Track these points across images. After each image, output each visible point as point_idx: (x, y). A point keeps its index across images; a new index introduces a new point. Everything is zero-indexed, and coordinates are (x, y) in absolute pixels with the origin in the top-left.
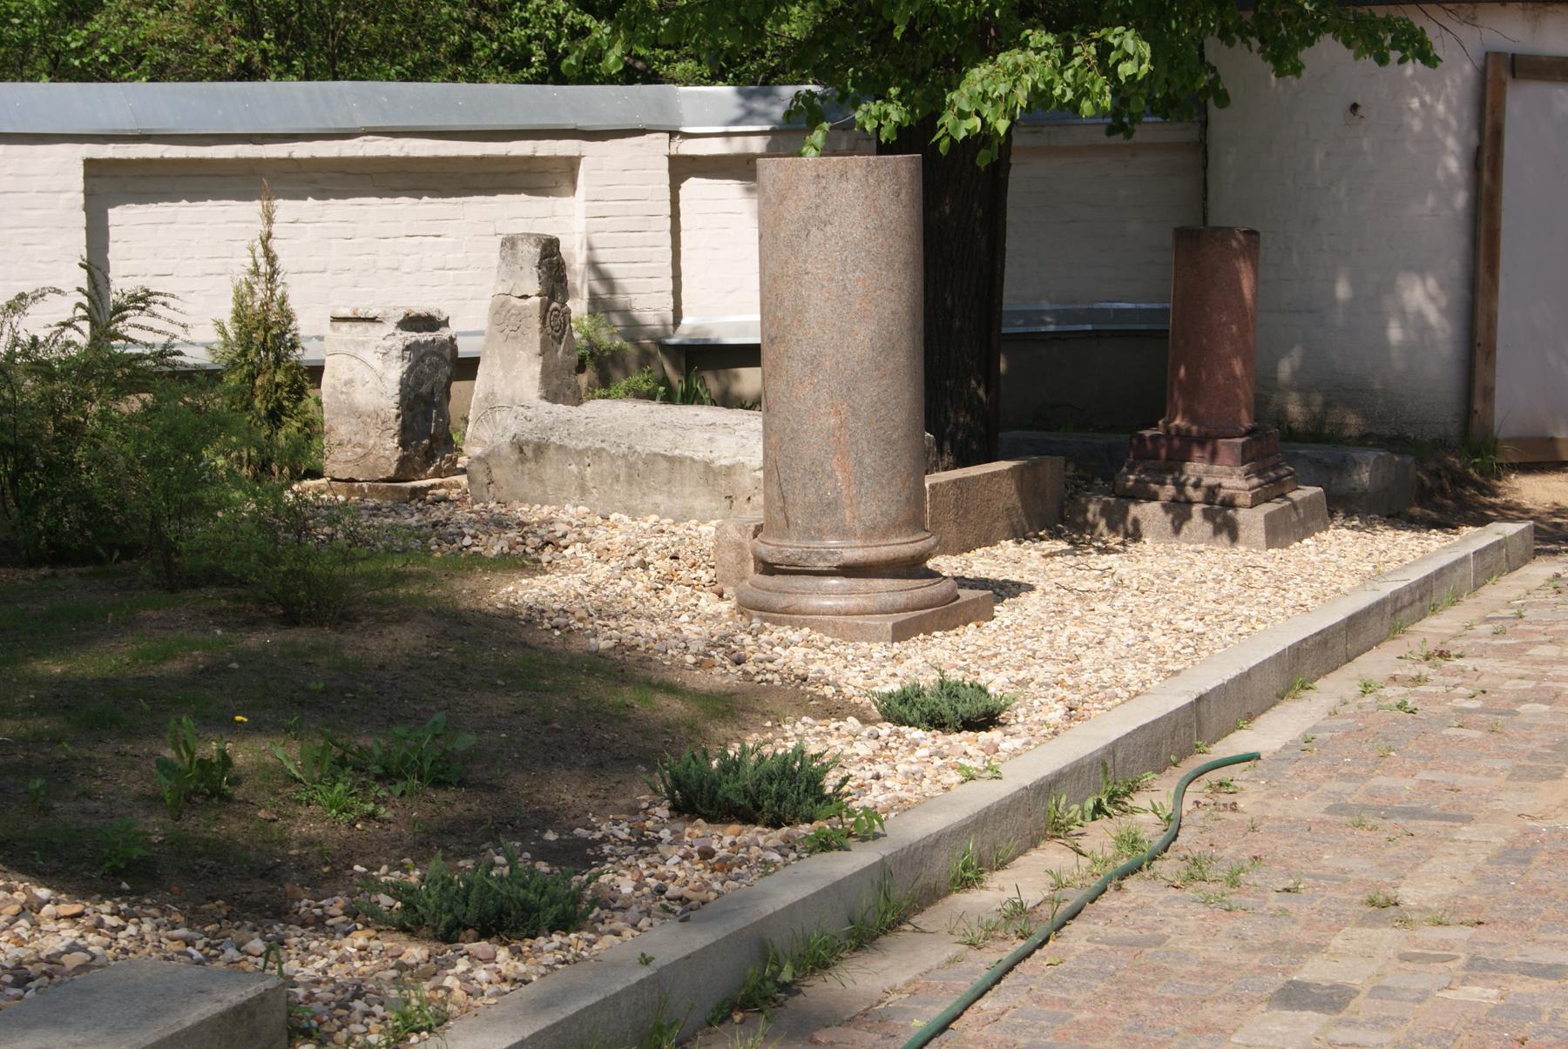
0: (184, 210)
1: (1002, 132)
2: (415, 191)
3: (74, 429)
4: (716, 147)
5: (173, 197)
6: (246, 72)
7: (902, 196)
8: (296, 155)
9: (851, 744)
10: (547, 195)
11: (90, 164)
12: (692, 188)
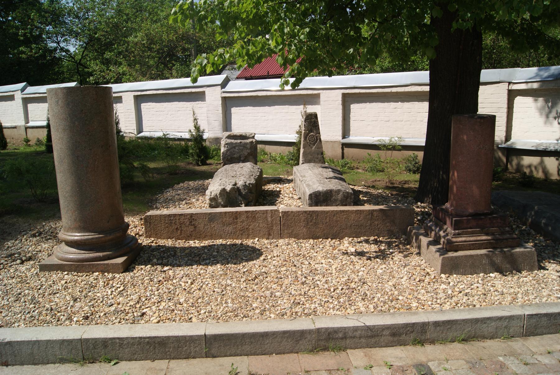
0: (368, 105)
1: (294, 79)
4: (523, 87)
7: (60, 103)
11: (134, 96)
12: (145, 106)
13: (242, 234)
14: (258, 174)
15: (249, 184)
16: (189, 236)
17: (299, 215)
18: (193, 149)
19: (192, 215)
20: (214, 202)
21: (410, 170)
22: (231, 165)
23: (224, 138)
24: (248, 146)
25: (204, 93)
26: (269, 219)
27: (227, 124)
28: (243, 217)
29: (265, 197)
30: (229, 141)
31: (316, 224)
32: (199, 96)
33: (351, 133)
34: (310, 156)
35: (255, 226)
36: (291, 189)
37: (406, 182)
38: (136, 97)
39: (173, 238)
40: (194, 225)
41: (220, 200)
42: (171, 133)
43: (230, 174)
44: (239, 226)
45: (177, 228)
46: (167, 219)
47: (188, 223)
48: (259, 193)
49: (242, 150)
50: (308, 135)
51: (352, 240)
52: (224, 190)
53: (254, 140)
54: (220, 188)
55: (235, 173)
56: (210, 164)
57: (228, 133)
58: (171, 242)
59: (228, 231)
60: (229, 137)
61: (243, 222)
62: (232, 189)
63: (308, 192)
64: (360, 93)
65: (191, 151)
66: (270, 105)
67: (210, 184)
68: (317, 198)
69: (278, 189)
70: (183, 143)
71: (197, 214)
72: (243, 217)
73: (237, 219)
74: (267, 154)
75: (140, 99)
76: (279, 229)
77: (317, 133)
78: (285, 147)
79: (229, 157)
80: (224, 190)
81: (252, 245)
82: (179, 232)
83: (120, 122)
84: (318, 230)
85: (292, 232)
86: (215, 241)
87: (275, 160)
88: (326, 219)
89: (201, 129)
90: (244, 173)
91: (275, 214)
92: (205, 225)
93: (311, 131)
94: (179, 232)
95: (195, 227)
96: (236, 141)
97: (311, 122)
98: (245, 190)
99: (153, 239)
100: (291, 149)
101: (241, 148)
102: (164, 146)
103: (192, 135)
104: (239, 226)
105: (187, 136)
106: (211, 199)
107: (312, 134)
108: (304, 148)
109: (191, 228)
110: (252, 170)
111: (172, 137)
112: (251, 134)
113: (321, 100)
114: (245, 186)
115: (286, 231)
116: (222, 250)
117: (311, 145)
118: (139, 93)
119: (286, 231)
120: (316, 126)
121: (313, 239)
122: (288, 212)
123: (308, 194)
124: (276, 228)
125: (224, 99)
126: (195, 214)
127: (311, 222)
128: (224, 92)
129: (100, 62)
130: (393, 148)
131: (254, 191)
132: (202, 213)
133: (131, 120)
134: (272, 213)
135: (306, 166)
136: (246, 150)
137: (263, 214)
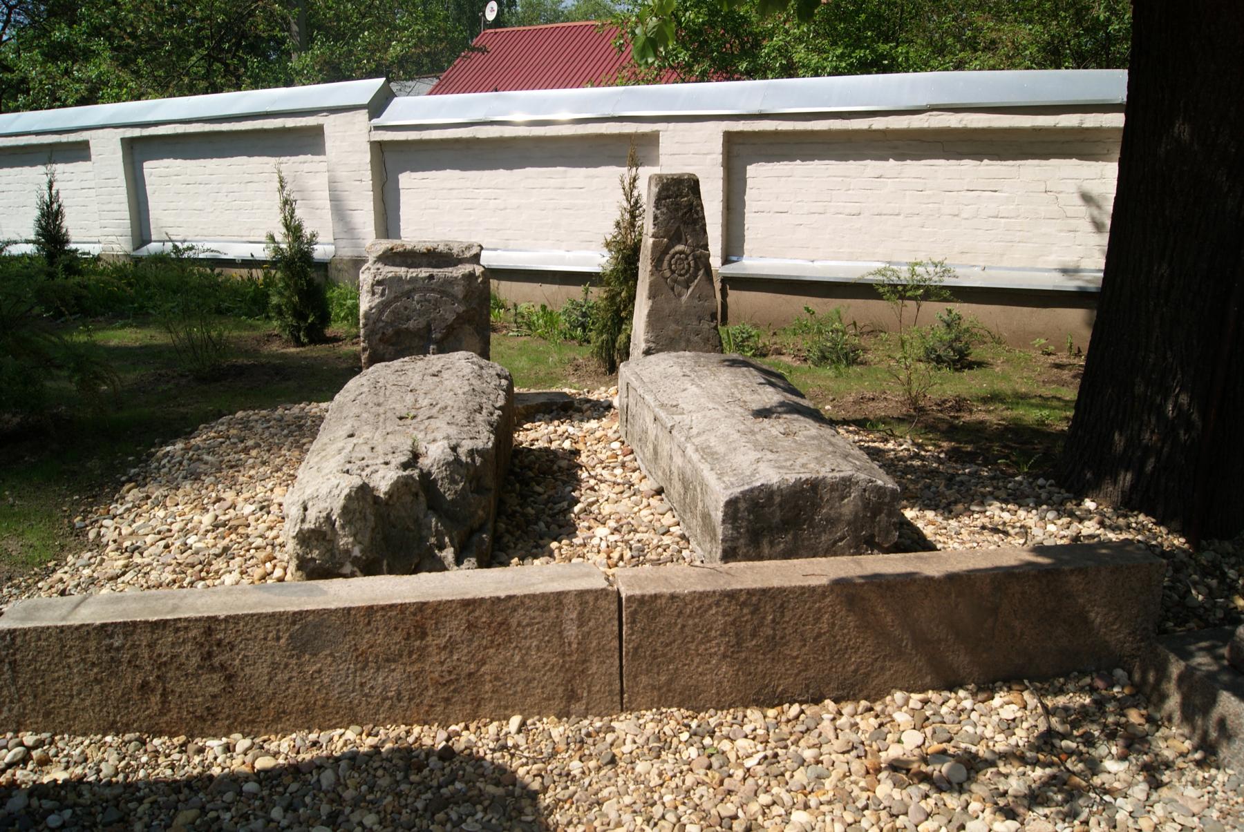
2: (978, 155)
3: (269, 451)
5: (791, 158)
6: (993, 68)
8: (875, 127)
9: (112, 658)
10: (1097, 160)
12: (154, 170)
13: (447, 700)
14: (501, 402)
15: (471, 453)
16: (202, 719)
17: (702, 612)
18: (281, 294)
19: (210, 625)
20: (320, 556)
21: (939, 360)
22: (397, 363)
23: (371, 259)
24: (459, 290)
25: (318, 131)
26: (572, 631)
27: (387, 220)
28: (454, 628)
29: (525, 483)
30: (389, 271)
31: (774, 644)
32: (304, 140)
33: (746, 246)
34: (673, 326)
35: (507, 661)
36: (616, 445)
37: (960, 404)
38: (130, 145)
39: (127, 728)
40: (223, 667)
41: (345, 541)
42: (199, 246)
43: (390, 404)
44: (434, 665)
45: (144, 686)
46: (92, 644)
47: (195, 660)
48: (514, 498)
49: (437, 304)
50: (665, 251)
51: (925, 702)
52: (364, 492)
53: (479, 270)
54: (349, 483)
55: (409, 398)
56: (336, 339)
57: (386, 244)
58: (112, 758)
59: (385, 688)
60: (389, 257)
61: (451, 646)
62: (400, 486)
63: (718, 492)
64: (776, 133)
65: (275, 300)
66: (510, 166)
67: (322, 419)
68: (765, 521)
69: (567, 445)
70: (258, 274)
71: (236, 619)
72: (454, 628)
73: (423, 635)
74: (502, 307)
75: (140, 149)
76: (615, 670)
77: (698, 246)
78: (555, 288)
79: (390, 331)
80: (364, 492)
81: (501, 759)
82: (155, 699)
83: (66, 211)
84: (779, 668)
85: (670, 682)
86: (324, 737)
87: (530, 325)
88: (817, 620)
89: (307, 231)
90: (448, 399)
91: (596, 608)
92: (274, 666)
93: (676, 238)
94: (155, 699)
95: (229, 678)
96: (413, 272)
97: (677, 207)
98: (453, 481)
99: (29, 739)
100: (597, 294)
101: (432, 295)
102: (167, 283)
103: (278, 250)
104: (434, 665)
105: (262, 252)
106: (304, 538)
107: (680, 247)
108: (652, 295)
109: (212, 684)
110: (476, 382)
111: (201, 256)
112: (469, 248)
113: (661, 150)
114: (455, 465)
115: (644, 679)
116: (355, 805)
117: (678, 288)
118: (137, 132)
119: (644, 679)
120: (695, 222)
121: (764, 702)
122: (655, 597)
123: (723, 499)
124: (601, 670)
125: (380, 150)
126: (227, 619)
127: (754, 635)
128: (377, 128)
129: (43, 54)
130: (900, 292)
131: (489, 481)
132: (259, 617)
133: (116, 207)
134: (584, 603)
135: (665, 362)
136: (451, 306)
137: (545, 609)
